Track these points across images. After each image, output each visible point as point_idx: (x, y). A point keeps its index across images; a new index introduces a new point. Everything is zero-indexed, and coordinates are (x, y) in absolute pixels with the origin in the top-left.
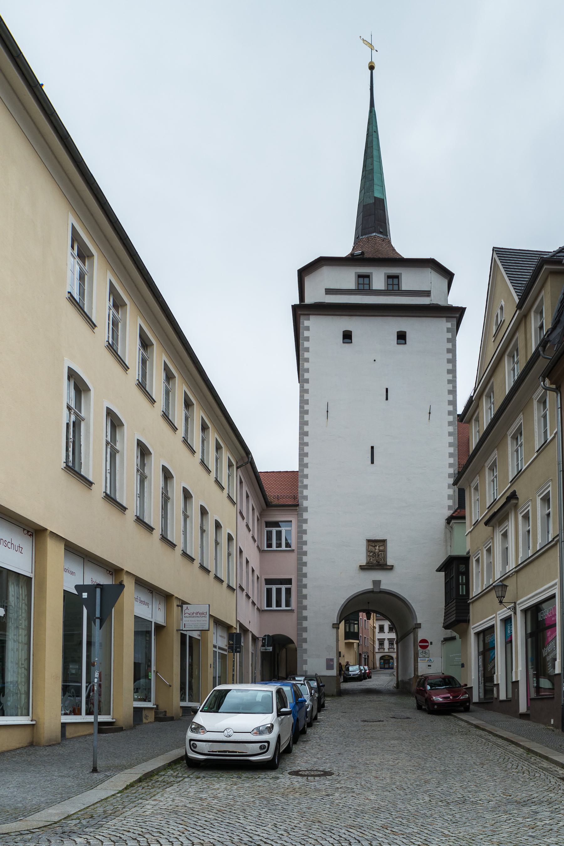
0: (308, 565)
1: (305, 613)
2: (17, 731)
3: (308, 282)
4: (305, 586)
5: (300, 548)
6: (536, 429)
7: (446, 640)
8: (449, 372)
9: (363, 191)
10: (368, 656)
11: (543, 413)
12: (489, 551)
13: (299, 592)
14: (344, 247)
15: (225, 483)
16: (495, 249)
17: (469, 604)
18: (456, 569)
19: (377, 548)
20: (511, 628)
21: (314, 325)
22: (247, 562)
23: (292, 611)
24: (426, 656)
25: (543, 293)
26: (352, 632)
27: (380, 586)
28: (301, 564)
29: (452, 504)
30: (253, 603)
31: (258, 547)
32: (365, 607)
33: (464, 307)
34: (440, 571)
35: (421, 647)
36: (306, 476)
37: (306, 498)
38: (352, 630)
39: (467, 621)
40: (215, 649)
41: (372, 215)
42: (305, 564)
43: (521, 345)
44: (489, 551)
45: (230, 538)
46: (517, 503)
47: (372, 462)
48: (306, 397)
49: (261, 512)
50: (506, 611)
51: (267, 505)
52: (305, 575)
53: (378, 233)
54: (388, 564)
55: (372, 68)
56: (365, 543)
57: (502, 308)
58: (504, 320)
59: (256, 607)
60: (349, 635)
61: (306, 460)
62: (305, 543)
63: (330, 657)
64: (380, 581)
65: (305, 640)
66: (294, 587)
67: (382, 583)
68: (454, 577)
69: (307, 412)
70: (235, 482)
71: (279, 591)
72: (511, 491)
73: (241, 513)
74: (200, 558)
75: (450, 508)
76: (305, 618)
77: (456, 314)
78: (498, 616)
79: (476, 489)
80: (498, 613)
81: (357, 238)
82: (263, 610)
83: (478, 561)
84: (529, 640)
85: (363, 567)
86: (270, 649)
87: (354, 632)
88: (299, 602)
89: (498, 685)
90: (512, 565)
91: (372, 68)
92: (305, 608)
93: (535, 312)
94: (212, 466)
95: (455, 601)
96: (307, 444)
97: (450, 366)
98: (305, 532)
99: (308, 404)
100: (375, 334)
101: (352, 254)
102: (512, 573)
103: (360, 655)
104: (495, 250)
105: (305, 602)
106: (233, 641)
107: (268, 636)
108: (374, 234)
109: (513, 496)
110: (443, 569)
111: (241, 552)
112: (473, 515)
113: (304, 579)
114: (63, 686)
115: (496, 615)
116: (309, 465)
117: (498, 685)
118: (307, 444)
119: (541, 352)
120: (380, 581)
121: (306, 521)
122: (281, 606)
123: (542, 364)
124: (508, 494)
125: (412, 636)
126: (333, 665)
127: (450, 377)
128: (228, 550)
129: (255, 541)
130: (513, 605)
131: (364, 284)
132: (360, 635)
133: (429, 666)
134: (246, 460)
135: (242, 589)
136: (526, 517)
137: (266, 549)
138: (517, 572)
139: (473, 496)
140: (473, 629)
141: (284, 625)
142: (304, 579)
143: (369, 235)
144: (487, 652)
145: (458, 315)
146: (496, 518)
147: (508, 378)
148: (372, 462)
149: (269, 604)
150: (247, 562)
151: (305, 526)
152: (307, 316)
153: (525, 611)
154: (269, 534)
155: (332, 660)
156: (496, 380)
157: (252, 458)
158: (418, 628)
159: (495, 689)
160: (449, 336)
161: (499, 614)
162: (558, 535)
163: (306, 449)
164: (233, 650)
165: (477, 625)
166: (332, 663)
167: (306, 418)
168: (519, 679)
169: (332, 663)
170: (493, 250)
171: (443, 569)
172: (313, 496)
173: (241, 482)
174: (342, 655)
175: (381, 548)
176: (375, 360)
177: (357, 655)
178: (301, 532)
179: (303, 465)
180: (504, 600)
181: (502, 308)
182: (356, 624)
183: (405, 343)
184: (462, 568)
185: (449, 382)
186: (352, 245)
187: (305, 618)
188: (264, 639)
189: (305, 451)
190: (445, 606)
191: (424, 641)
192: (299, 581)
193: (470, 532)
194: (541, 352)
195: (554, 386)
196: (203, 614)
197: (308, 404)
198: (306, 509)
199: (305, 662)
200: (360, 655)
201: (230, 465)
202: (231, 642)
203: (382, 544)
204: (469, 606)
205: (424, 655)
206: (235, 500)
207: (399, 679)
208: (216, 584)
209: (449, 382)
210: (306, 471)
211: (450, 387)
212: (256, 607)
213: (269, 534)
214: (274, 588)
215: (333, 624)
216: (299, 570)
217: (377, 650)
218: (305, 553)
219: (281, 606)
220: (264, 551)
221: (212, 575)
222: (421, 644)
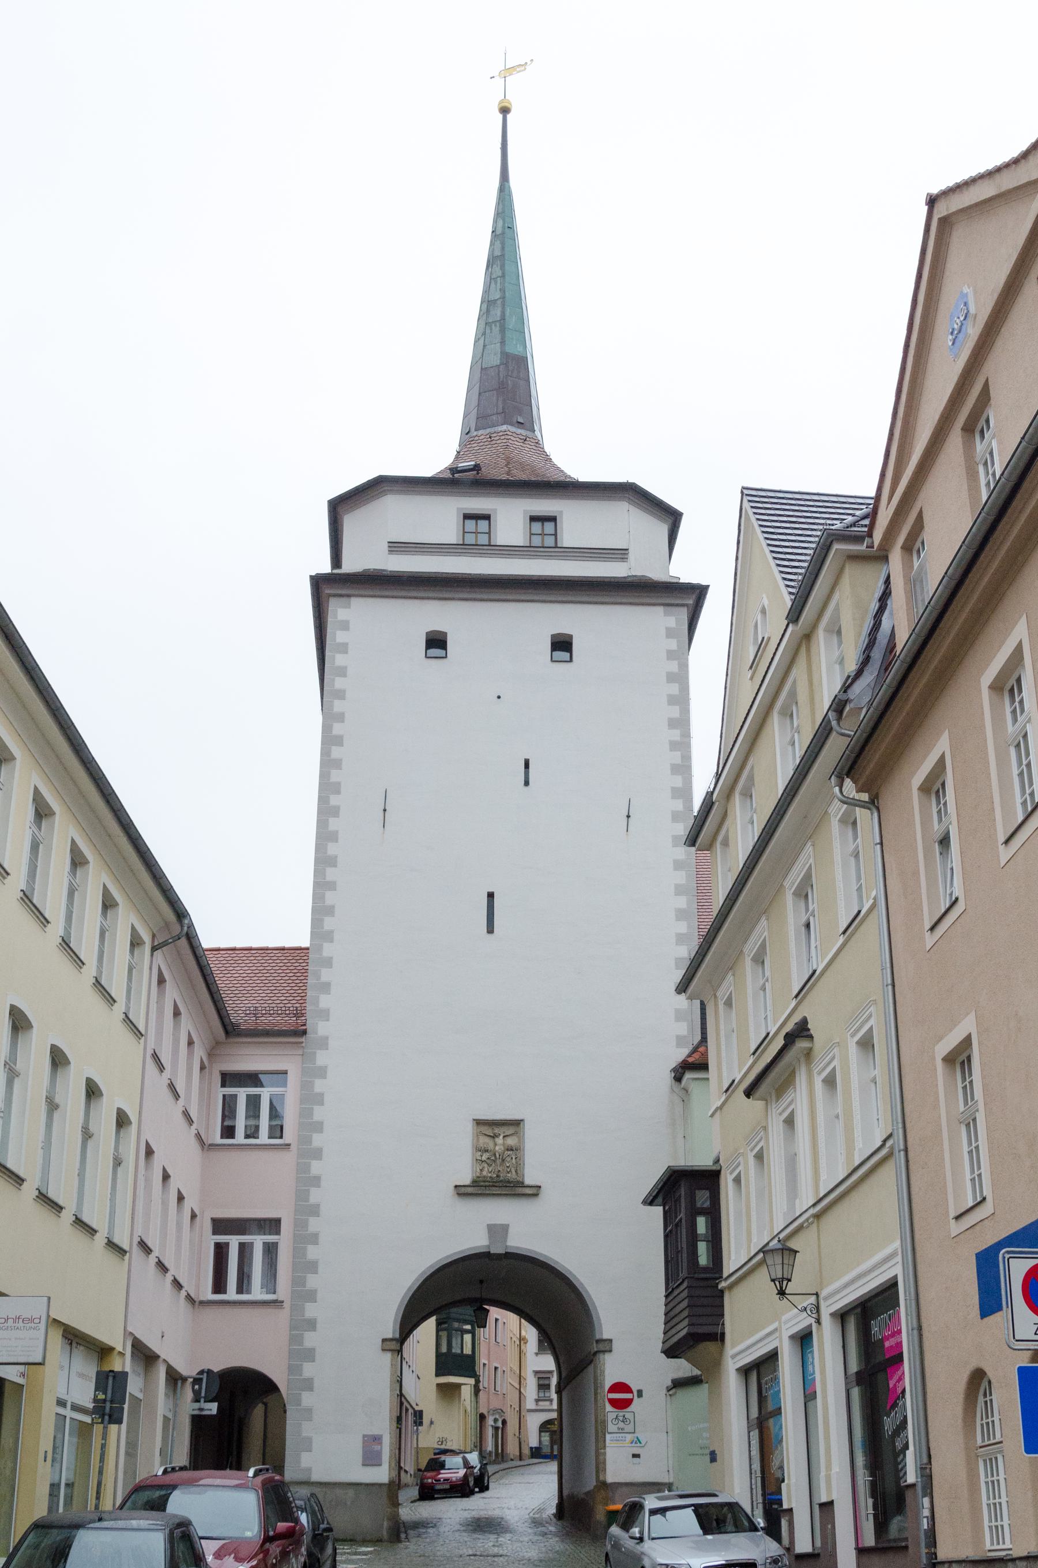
0: (323, 1183)
1: (311, 1310)
3: (350, 523)
4: (314, 1239)
5: (305, 1140)
6: (840, 885)
7: (679, 1384)
8: (673, 723)
9: (481, 342)
10: (504, 1422)
11: (852, 847)
12: (760, 1157)
13: (299, 1252)
14: (435, 452)
15: (117, 990)
16: (746, 492)
17: (722, 1292)
18: (688, 1195)
19: (500, 1140)
20: (813, 1358)
21: (358, 616)
22: (166, 1177)
23: (277, 1303)
24: (629, 1428)
25: (836, 596)
26: (456, 1355)
28: (307, 1181)
29: (685, 1033)
30: (177, 1284)
31: (198, 1136)
33: (704, 583)
34: (651, 1203)
35: (614, 1403)
36: (328, 962)
37: (325, 1015)
38: (456, 1350)
39: (719, 1338)
40: (61, 1410)
41: (503, 387)
43: (802, 696)
44: (760, 1157)
45: (122, 1120)
46: (811, 1049)
47: (490, 930)
48: (335, 776)
49: (213, 1048)
50: (795, 1316)
51: (227, 1033)
52: (315, 1211)
53: (512, 424)
54: (528, 1181)
55: (505, 111)
56: (470, 1127)
57: (763, 611)
58: (769, 639)
59: (183, 1293)
61: (329, 923)
62: (319, 1127)
64: (505, 1228)
65: (308, 1385)
66: (284, 1240)
68: (683, 1221)
69: (335, 812)
70: (146, 979)
71: (245, 1250)
72: (797, 1018)
73: (155, 1056)
74: (38, 1175)
75: (680, 1041)
76: (311, 1325)
77: (695, 596)
78: (784, 1327)
79: (729, 1003)
80: (784, 1318)
81: (466, 432)
82: (202, 1303)
83: (737, 1180)
84: (856, 1392)
85: (463, 1190)
86: (212, 1408)
87: (462, 1355)
88: (298, 1281)
89: (790, 1510)
90: (806, 1199)
91: (505, 111)
92: (311, 1296)
93: (827, 630)
94: (87, 949)
96: (332, 886)
97: (675, 712)
99: (338, 792)
100: (499, 638)
101: (453, 470)
102: (807, 1220)
103: (482, 1417)
104: (746, 492)
105: (312, 1281)
106: (105, 1393)
107: (209, 1372)
108: (504, 427)
109: (801, 1031)
110: (660, 1199)
111: (149, 1152)
112: (724, 1069)
115: (780, 1323)
116: (336, 937)
117: (790, 1510)
118: (332, 886)
119: (834, 723)
120: (505, 1228)
121: (322, 1073)
122: (249, 1292)
123: (835, 748)
124: (789, 1027)
125: (591, 1368)
127: (676, 735)
128: (116, 1148)
129: (190, 1121)
130: (812, 1299)
131: (476, 533)
132: (483, 1361)
133: (635, 1456)
134: (176, 929)
135: (145, 1248)
136: (830, 1082)
137: (218, 1140)
138: (818, 1216)
139: (722, 1022)
140: (733, 1357)
141: (247, 1342)
143: (492, 430)
144: (764, 1422)
145: (691, 602)
146: (767, 1081)
147: (779, 758)
148: (490, 930)
149: (219, 1285)
150: (166, 1177)
151: (319, 1085)
152: (344, 599)
153: (842, 1316)
154: (229, 1106)
155: (377, 1439)
156: (758, 762)
157: (191, 926)
158: (604, 1352)
159: (784, 1523)
160: (673, 644)
161: (785, 1323)
162: (890, 1136)
163: (330, 898)
164: (103, 1416)
165: (740, 1348)
166: (377, 1448)
167: (333, 824)
168: (834, 1497)
169: (377, 1448)
170: (742, 492)
171: (660, 1199)
172: (339, 1011)
173: (161, 981)
174: (426, 1420)
175: (511, 1141)
176: (499, 697)
177: (473, 1420)
178: (311, 1099)
179: (318, 931)
180: (790, 1288)
181: (763, 611)
182: (467, 1332)
183: (571, 660)
184: (703, 1198)
185: (674, 746)
186: (456, 447)
187: (311, 1325)
188: (197, 1381)
190: (666, 1297)
191: (620, 1387)
192: (300, 1224)
193: (720, 1108)
194: (834, 723)
195: (865, 797)
196: (31, 1320)
197: (338, 792)
198: (324, 1043)
199: (307, 1445)
200: (482, 1417)
201: (136, 942)
202: (101, 1396)
203: (510, 1130)
204: (722, 1297)
205: (621, 1425)
206: (142, 1029)
207: (565, 1493)
208: (79, 1238)
209: (674, 746)
211: (676, 757)
212: (183, 1293)
213: (229, 1106)
214: (234, 1242)
216: (301, 1196)
217: (530, 1403)
219: (249, 1292)
220: (213, 1146)
221: (67, 1216)
222: (628, 1396)
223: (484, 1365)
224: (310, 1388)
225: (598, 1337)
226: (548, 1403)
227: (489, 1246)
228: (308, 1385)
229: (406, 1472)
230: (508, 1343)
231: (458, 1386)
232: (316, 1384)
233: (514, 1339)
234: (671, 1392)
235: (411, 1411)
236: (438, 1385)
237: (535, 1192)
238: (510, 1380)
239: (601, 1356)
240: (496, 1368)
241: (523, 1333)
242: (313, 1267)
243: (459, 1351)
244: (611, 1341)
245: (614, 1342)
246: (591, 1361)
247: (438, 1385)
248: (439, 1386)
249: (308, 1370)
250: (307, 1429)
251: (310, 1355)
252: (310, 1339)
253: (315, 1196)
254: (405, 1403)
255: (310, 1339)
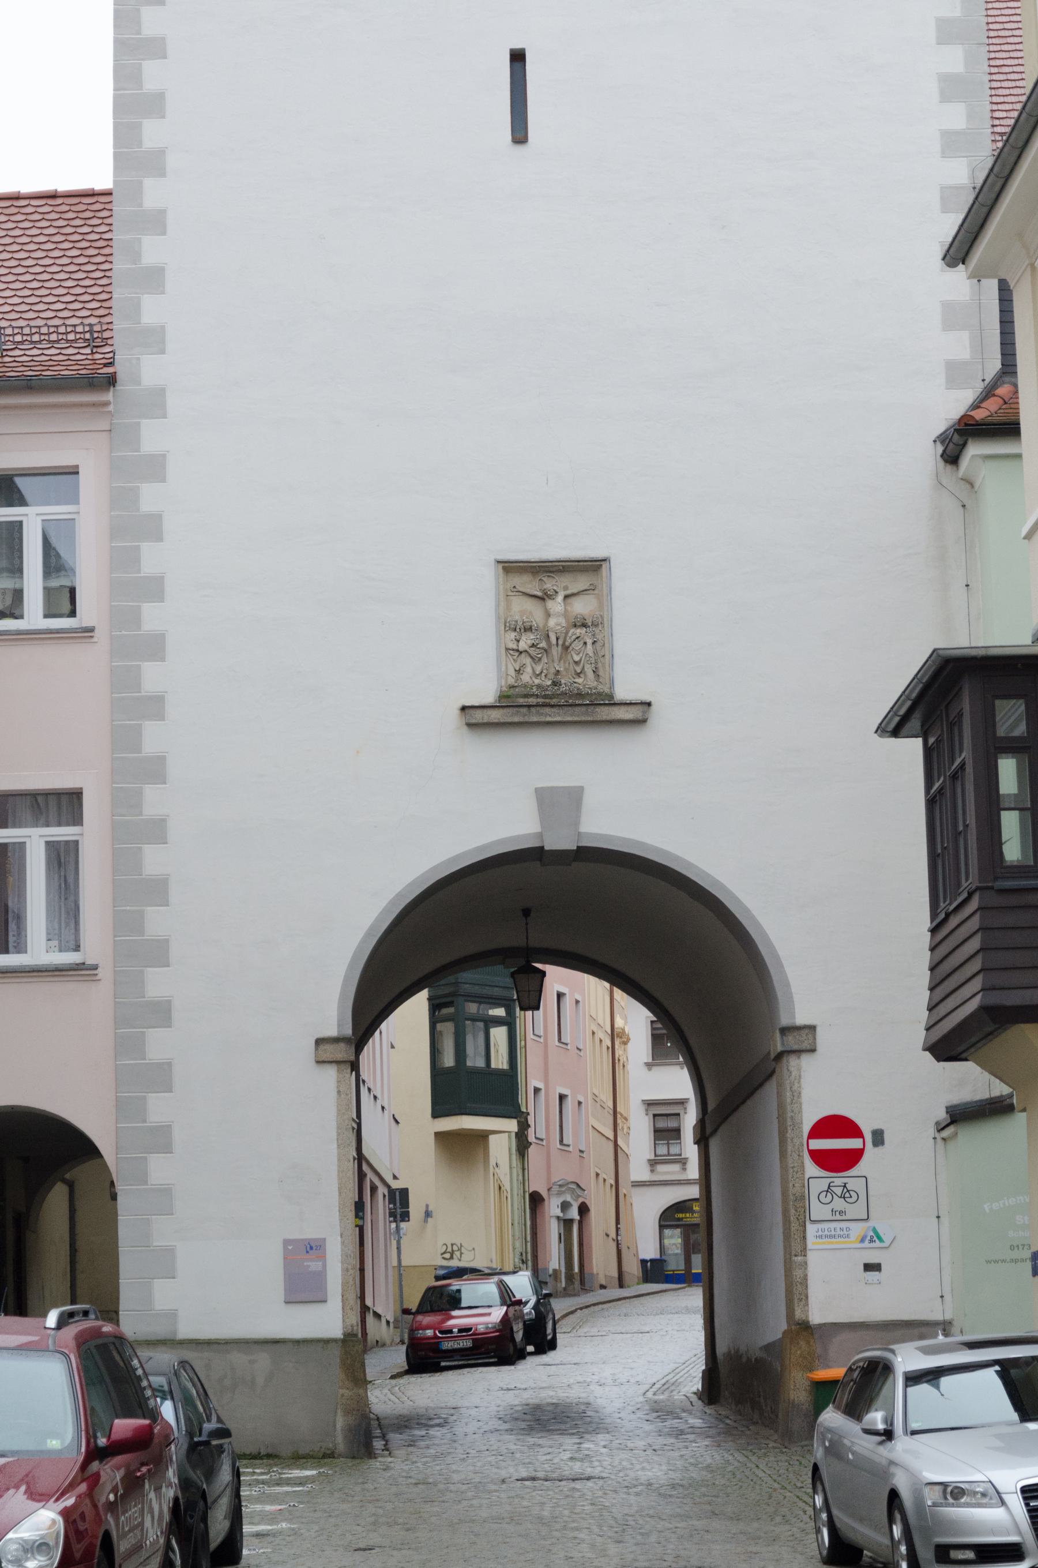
1: (157, 984)
2: (1006, 806)
7: (961, 1116)
10: (583, 1209)
19: (556, 605)
23: (83, 970)
24: (857, 1210)
26: (475, 1072)
27: (577, 823)
28: (134, 706)
32: (512, 937)
34: (896, 733)
35: (822, 1159)
36: (157, 222)
38: (475, 1060)
42: (155, 706)
47: (520, 135)
52: (155, 770)
54: (621, 693)
56: (488, 577)
60: (467, 1089)
63: (310, 1233)
64: (574, 797)
65: (161, 1139)
66: (92, 836)
67: (589, 801)
68: (969, 769)
76: (161, 1013)
85: (479, 716)
87: (488, 1073)
88: (126, 924)
92: (158, 953)
95: (974, 904)
98: (152, 528)
103: (536, 1200)
105: (157, 921)
110: (915, 723)
113: (151, 793)
114: (115, 153)
116: (172, 161)
118: (157, 48)
120: (574, 797)
121: (155, 468)
125: (771, 1087)
126: (320, 1277)
132: (534, 1082)
133: (869, 1267)
142: (151, 793)
148: (520, 135)
151: (150, 497)
155: (314, 1248)
158: (798, 1052)
166: (315, 1266)
171: (915, 723)
174: (415, 1209)
175: (582, 607)
177: (516, 1208)
178: (134, 528)
182: (498, 1022)
187: (161, 1013)
189: (150, 85)
190: (933, 931)
192: (126, 800)
198: (156, 403)
199: (166, 1264)
200: (536, 1200)
203: (581, 582)
205: (839, 1204)
207: (721, 1349)
210: (154, 193)
215: (319, 1042)
216: (124, 739)
217: (637, 1169)
218: (155, 647)
222: (818, 1144)
223: (537, 1090)
224: (167, 1148)
225: (785, 1021)
226: (676, 1167)
227: (540, 835)
228: (161, 1139)
229: (377, 1316)
230: (587, 1044)
231: (483, 1136)
232: (178, 1136)
233: (600, 1034)
234: (946, 1133)
235: (382, 1190)
236: (438, 1135)
237: (638, 715)
238: (593, 1122)
239: (793, 1061)
240: (562, 1098)
241: (619, 1022)
242: (158, 891)
243: (481, 1063)
244: (812, 1028)
245: (819, 1031)
246: (773, 1072)
247: (438, 1135)
248: (443, 1138)
249: (159, 1108)
250: (163, 1232)
251: (161, 1077)
252: (159, 1045)
253: (154, 738)
254: (370, 1175)
255: (159, 1045)
